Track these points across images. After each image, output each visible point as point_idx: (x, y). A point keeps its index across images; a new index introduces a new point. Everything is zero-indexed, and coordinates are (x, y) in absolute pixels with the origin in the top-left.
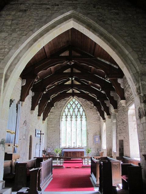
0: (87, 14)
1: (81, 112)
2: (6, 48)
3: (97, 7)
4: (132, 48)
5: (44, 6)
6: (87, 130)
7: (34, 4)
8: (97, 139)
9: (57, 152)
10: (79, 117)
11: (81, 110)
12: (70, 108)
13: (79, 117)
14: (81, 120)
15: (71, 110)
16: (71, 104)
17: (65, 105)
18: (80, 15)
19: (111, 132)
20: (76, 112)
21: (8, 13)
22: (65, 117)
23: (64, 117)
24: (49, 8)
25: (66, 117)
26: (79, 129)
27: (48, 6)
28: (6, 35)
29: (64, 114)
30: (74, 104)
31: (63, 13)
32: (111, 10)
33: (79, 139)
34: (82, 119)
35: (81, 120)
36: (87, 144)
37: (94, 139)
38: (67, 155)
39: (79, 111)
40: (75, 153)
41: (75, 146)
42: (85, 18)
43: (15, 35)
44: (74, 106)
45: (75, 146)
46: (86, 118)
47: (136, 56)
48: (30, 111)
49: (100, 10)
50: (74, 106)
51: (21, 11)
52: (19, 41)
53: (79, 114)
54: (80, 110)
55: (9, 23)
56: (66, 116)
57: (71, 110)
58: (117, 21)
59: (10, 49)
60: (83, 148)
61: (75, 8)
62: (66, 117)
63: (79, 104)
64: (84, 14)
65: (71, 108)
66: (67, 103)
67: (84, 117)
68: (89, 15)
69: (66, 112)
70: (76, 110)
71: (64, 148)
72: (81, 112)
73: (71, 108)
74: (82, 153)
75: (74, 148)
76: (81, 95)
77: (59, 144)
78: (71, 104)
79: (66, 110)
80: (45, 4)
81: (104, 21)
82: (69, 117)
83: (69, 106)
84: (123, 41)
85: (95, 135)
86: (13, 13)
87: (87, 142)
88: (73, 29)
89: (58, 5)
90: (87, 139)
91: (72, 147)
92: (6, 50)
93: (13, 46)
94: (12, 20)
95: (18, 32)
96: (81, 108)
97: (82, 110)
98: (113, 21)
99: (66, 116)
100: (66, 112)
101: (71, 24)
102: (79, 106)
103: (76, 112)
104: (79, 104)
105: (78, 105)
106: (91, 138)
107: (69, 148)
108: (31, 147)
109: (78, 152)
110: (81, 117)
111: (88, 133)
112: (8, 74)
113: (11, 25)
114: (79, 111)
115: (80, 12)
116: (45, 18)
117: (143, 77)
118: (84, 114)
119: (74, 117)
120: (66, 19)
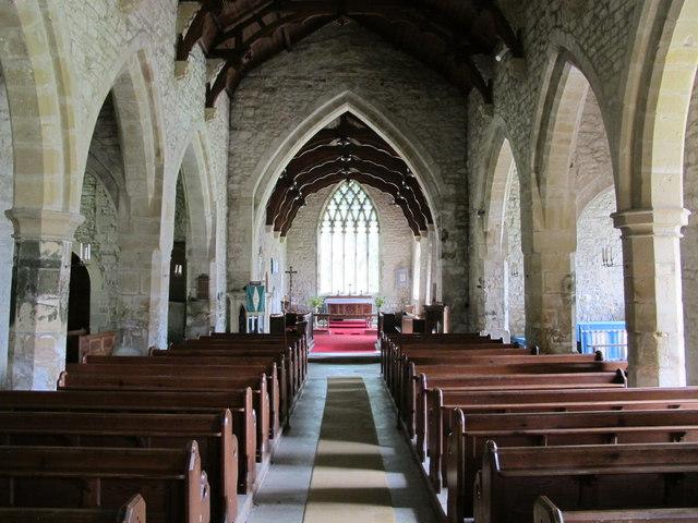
0: (370, 98)
1: (368, 213)
2: (251, 159)
3: (387, 83)
4: (435, 158)
5: (303, 82)
6: (381, 256)
7: (286, 77)
8: (403, 277)
9: (315, 304)
10: (362, 224)
11: (368, 207)
12: (341, 203)
13: (362, 224)
14: (367, 232)
15: (344, 208)
16: (344, 192)
17: (329, 197)
18: (360, 99)
19: (426, 258)
20: (356, 213)
21: (246, 93)
22: (329, 223)
23: (326, 224)
24: (310, 86)
25: (332, 225)
26: (362, 255)
27: (309, 83)
28: (249, 135)
29: (326, 217)
30: (350, 193)
31: (333, 96)
32: (407, 90)
33: (362, 274)
34: (370, 229)
35: (367, 232)
36: (381, 288)
37: (397, 275)
38: (335, 311)
39: (361, 210)
40: (351, 307)
41: (353, 291)
42: (368, 105)
43: (262, 136)
44: (350, 197)
45: (353, 291)
46: (378, 226)
47: (439, 172)
48: (264, 226)
49: (392, 90)
50: (350, 197)
51: (266, 90)
52: (269, 146)
53: (362, 217)
54: (364, 207)
55: (250, 113)
56: (332, 222)
57: (344, 208)
58: (417, 112)
59: (258, 160)
60: (370, 297)
61: (351, 87)
62: (332, 225)
63: (362, 193)
64: (366, 98)
65: (344, 202)
66: (334, 190)
67: (374, 224)
68: (373, 101)
69: (332, 213)
70: (356, 207)
71: (328, 297)
72: (368, 213)
73: (344, 202)
74: (368, 308)
75: (349, 297)
76: (362, 180)
77: (316, 287)
78: (344, 192)
79: (332, 207)
80: (304, 78)
81: (395, 111)
82: (338, 224)
83: (338, 197)
84: (422, 147)
85: (400, 267)
86: (255, 94)
87: (380, 283)
88: (348, 114)
89: (324, 80)
90: (381, 277)
91: (346, 294)
92: (253, 161)
93: (262, 154)
94: (256, 108)
95: (267, 131)
96: (368, 202)
97: (371, 207)
98: (411, 112)
99: (332, 222)
100: (332, 213)
101: (346, 108)
102: (362, 196)
103: (356, 213)
104: (362, 193)
105: (359, 196)
106: (389, 275)
107: (338, 297)
108: (651, 292)
109: (359, 305)
110: (367, 226)
111: (382, 263)
112: (258, 197)
113: (253, 118)
114: (361, 210)
115: (359, 94)
116: (306, 104)
117: (446, 204)
118: (374, 217)
119: (350, 224)
120: (337, 105)
